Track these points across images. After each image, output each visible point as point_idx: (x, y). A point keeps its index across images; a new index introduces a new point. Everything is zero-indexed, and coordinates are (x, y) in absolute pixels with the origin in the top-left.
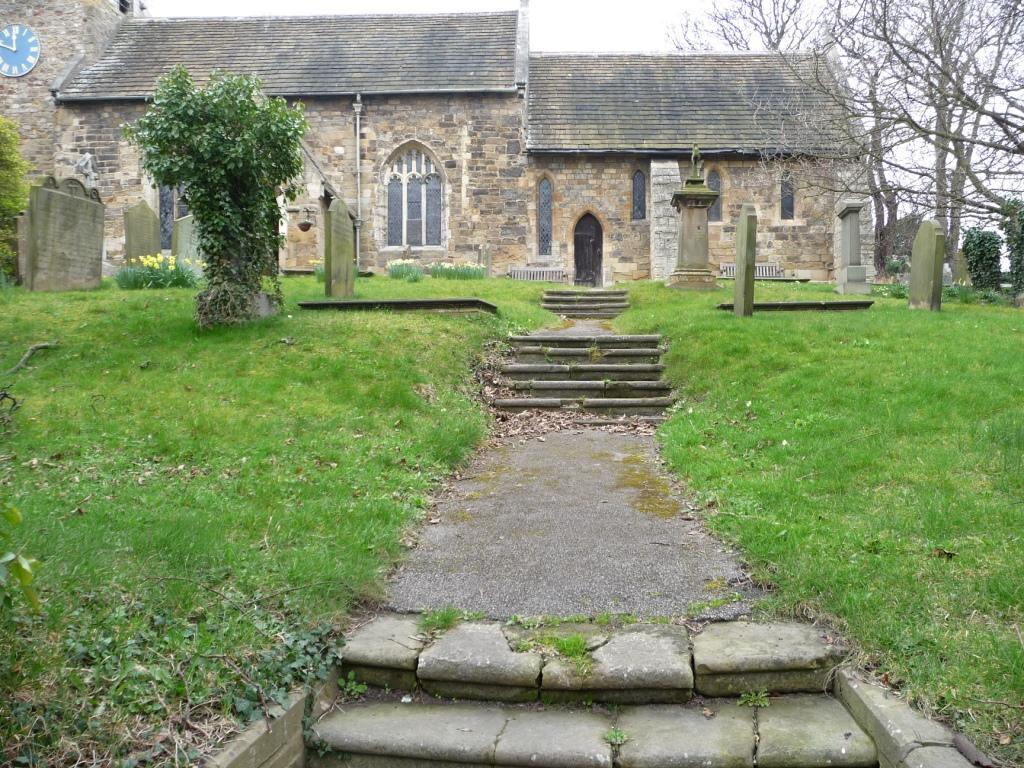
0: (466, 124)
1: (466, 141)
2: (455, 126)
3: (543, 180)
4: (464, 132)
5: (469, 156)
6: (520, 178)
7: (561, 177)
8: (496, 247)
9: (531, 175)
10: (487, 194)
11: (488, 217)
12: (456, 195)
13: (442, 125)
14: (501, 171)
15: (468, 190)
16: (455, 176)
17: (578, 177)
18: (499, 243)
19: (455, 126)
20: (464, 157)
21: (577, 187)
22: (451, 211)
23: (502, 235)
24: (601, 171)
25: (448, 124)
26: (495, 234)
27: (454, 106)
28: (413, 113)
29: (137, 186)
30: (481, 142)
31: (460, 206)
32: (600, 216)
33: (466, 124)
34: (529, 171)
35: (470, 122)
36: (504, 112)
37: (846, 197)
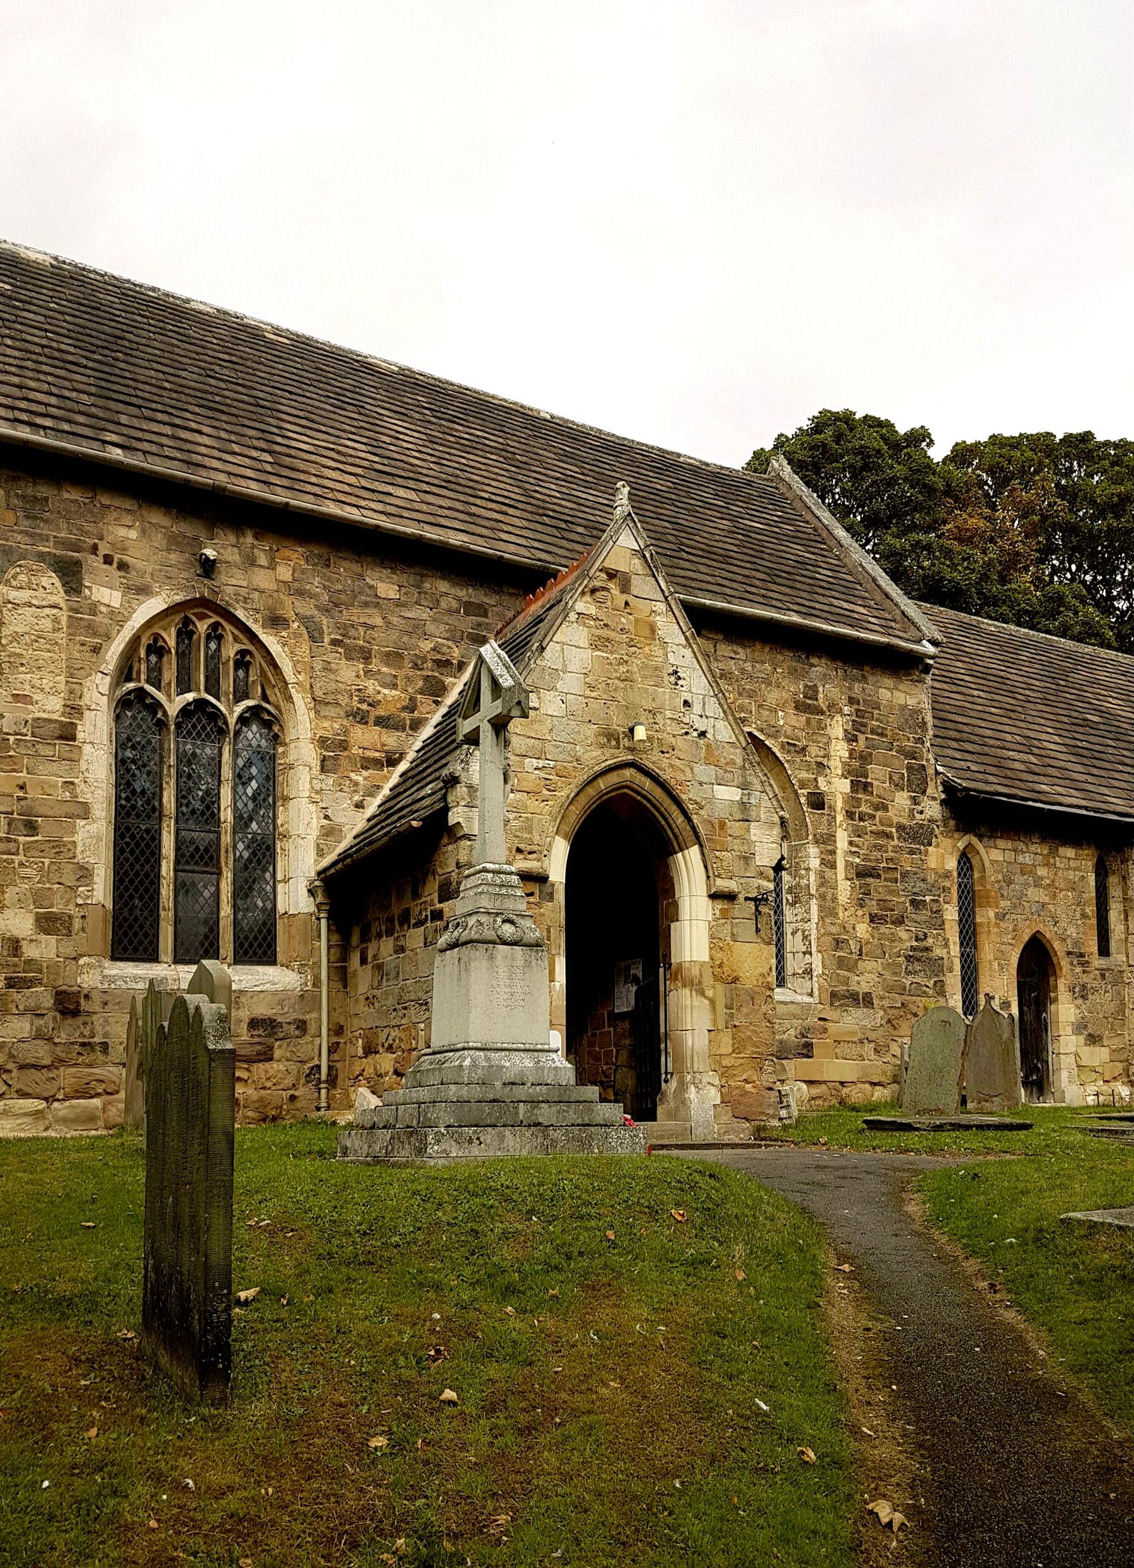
0: (840, 712)
1: (840, 750)
2: (822, 713)
3: (965, 860)
4: (837, 727)
5: (844, 786)
6: (930, 849)
7: (996, 855)
8: (898, 1000)
9: (946, 842)
10: (879, 876)
11: (883, 929)
12: (829, 873)
13: (799, 707)
14: (901, 828)
15: (848, 864)
16: (823, 829)
17: (1020, 859)
18: (902, 991)
19: (822, 713)
20: (838, 787)
21: (1019, 879)
22: (821, 908)
23: (908, 973)
24: (1053, 853)
25: (806, 706)
26: (892, 967)
27: (820, 668)
28: (748, 666)
29: (61, 747)
30: (865, 758)
31: (834, 899)
32: (1057, 945)
33: (840, 712)
34: (947, 834)
35: (846, 710)
36: (900, 698)
37: (281, 997)
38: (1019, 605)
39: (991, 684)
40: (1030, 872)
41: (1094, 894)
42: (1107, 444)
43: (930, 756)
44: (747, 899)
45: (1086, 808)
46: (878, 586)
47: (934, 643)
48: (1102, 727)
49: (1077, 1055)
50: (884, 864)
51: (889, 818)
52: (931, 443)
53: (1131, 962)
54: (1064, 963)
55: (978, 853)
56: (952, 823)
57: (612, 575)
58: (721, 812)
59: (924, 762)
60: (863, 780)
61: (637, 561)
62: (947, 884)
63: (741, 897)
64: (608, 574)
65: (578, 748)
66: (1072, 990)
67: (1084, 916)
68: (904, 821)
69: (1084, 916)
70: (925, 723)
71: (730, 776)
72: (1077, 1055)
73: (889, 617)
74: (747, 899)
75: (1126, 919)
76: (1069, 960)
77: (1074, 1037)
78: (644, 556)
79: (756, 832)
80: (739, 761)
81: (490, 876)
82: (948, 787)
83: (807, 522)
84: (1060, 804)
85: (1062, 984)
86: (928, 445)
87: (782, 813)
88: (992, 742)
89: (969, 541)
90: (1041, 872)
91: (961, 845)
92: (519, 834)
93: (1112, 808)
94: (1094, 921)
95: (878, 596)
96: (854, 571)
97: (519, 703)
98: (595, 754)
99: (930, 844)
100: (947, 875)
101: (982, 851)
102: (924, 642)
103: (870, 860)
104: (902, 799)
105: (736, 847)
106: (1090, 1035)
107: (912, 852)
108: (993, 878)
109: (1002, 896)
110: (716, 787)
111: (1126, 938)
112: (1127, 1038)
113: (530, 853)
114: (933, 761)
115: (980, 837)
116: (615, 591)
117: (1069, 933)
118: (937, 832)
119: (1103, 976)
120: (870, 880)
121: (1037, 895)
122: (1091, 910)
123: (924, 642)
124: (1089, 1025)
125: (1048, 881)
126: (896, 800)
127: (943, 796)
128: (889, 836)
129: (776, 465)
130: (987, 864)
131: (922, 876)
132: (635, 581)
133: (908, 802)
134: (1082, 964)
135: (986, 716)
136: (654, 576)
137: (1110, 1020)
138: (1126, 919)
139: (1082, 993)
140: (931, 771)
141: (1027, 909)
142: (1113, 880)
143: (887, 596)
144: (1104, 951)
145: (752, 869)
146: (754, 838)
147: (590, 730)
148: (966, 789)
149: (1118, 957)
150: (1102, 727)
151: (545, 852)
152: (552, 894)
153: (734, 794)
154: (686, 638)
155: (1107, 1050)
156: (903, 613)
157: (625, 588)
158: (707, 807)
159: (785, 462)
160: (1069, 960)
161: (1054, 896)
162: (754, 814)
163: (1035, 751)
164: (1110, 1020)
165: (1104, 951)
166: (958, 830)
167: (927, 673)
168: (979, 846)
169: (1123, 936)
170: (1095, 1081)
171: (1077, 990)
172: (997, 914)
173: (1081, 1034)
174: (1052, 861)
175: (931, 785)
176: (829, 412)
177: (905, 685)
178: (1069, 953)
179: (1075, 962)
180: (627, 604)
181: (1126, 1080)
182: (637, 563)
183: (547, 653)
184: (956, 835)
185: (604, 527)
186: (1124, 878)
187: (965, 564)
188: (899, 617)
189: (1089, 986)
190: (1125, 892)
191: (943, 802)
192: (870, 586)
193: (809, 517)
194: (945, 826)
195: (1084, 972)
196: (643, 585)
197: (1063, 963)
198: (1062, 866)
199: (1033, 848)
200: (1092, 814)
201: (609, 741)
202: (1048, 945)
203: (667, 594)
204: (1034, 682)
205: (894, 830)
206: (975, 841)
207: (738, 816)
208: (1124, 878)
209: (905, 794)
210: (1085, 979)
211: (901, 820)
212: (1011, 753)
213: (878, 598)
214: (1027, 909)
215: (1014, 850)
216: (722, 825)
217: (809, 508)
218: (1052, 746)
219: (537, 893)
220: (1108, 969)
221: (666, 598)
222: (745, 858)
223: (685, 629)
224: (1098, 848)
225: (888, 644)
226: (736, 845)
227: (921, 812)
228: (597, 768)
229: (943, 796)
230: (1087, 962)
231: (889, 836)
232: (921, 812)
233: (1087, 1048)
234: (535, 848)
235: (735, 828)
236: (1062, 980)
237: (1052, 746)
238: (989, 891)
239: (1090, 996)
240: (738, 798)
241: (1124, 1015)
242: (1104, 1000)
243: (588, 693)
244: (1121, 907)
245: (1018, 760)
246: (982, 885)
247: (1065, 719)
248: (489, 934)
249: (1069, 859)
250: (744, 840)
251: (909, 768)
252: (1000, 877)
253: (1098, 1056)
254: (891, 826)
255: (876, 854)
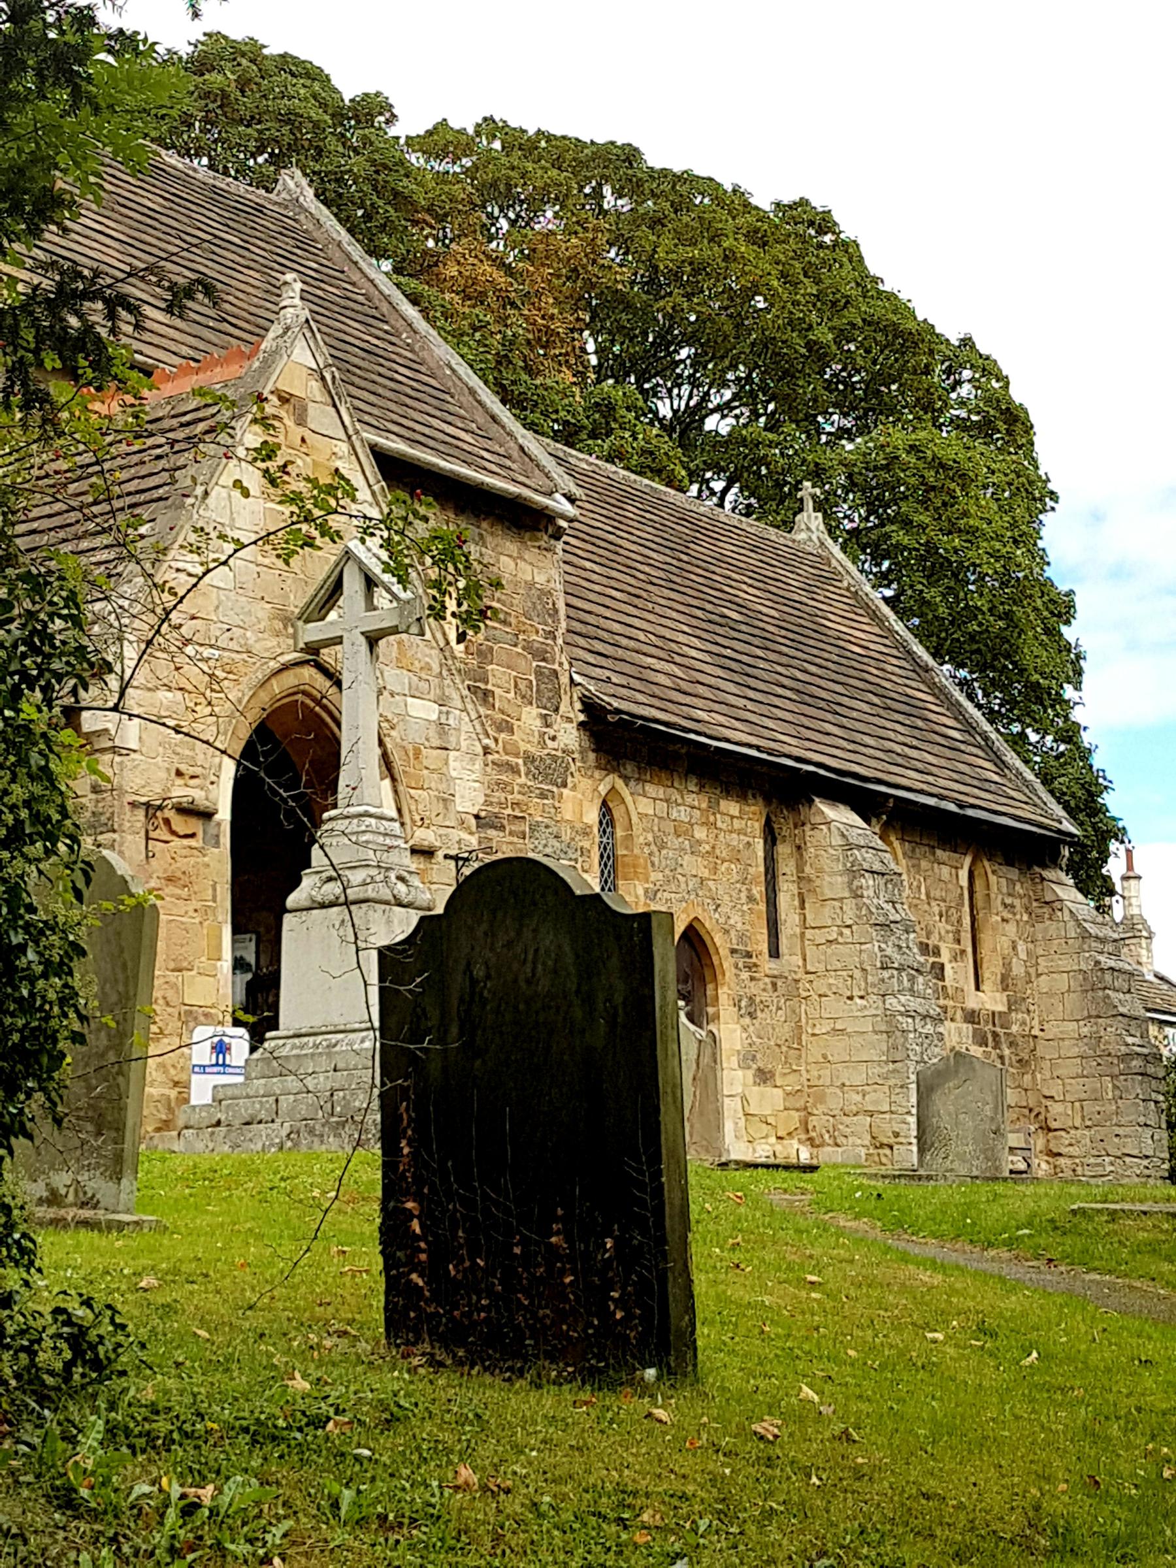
6: (565, 791)
7: (645, 806)
9: (585, 784)
10: (502, 828)
14: (529, 759)
21: (673, 841)
24: (713, 807)
32: (718, 939)
36: (526, 572)
38: (557, 412)
39: (601, 552)
40: (686, 833)
41: (762, 869)
42: (665, 173)
43: (564, 660)
44: (446, 857)
45: (758, 748)
46: (479, 402)
47: (571, 499)
48: (743, 628)
49: (744, 1098)
50: (509, 811)
51: (515, 744)
52: (392, 119)
53: (810, 968)
54: (727, 963)
55: (623, 801)
56: (592, 756)
57: (285, 399)
58: (415, 735)
59: (556, 667)
60: (482, 686)
61: (314, 383)
62: (586, 844)
63: (440, 854)
64: (280, 398)
65: (249, 634)
66: (737, 1004)
67: (751, 899)
68: (534, 750)
69: (751, 899)
70: (556, 611)
71: (425, 685)
72: (744, 1098)
73: (502, 451)
74: (446, 857)
75: (803, 907)
76: (732, 961)
77: (740, 1073)
78: (323, 378)
79: (456, 765)
80: (436, 668)
81: (373, 821)
82: (590, 707)
83: (353, 284)
84: (728, 740)
85: (723, 992)
86: (387, 122)
87: (486, 741)
88: (624, 642)
89: (481, 298)
90: (700, 833)
91: (603, 789)
92: (178, 749)
93: (787, 749)
94: (762, 907)
95: (481, 418)
96: (439, 373)
97: (419, 620)
98: (269, 644)
99: (565, 785)
100: (586, 831)
101: (629, 799)
102: (557, 496)
103: (491, 804)
104: (530, 717)
105: (433, 785)
106: (759, 1069)
107: (543, 796)
108: (641, 840)
109: (653, 864)
110: (410, 700)
111: (803, 934)
112: (805, 1075)
113: (192, 777)
114: (566, 666)
115: (626, 779)
116: (289, 422)
117: (732, 922)
118: (573, 768)
119: (774, 985)
120: (492, 833)
121: (693, 865)
122: (759, 890)
123: (557, 496)
124: (759, 1056)
125: (708, 848)
126: (523, 717)
127: (582, 717)
128: (515, 770)
129: (291, 184)
130: (635, 819)
131: (555, 830)
132: (313, 410)
133: (538, 722)
134: (749, 968)
135: (608, 602)
136: (335, 406)
137: (784, 1049)
138: (803, 907)
139: (750, 1009)
140: (564, 680)
141: (683, 886)
142: (783, 850)
143: (494, 418)
144: (775, 953)
145: (452, 815)
146: (454, 774)
147: (262, 611)
148: (618, 711)
149: (790, 959)
150: (743, 628)
151: (214, 778)
152: (218, 836)
153: (431, 711)
154: (373, 493)
155: (779, 1092)
156: (521, 448)
157: (301, 422)
158: (400, 727)
159: (304, 182)
160: (732, 961)
161: (715, 870)
162: (453, 739)
163: (678, 659)
164: (784, 1049)
165: (775, 953)
166: (598, 767)
167: (558, 539)
168: (625, 792)
169: (798, 930)
170: (766, 1137)
171: (743, 1004)
172: (646, 891)
173: (749, 1068)
174: (712, 819)
175: (565, 699)
176: (225, 38)
177: (531, 554)
178: (733, 951)
179: (741, 965)
180: (303, 440)
181: (804, 1137)
182: (315, 385)
183: (211, 501)
184: (597, 774)
185: (266, 324)
186: (799, 848)
187: (478, 336)
188: (515, 454)
189: (758, 1000)
190: (800, 868)
191: (581, 725)
192: (467, 399)
193: (356, 277)
194: (583, 760)
195: (752, 979)
196: (321, 417)
197: (726, 965)
198: (724, 826)
199: (690, 799)
200: (764, 756)
201: (285, 627)
202: (706, 938)
203: (351, 432)
204: (654, 555)
205: (520, 761)
206: (620, 784)
207: (436, 742)
208: (799, 848)
209: (535, 711)
210: (754, 989)
211: (529, 747)
212: (650, 660)
213: (481, 420)
214: (683, 886)
215: (667, 801)
216: (417, 754)
217: (356, 263)
218: (694, 653)
219: (200, 835)
220: (781, 976)
221: (349, 437)
222: (444, 800)
223: (372, 481)
224: (768, 801)
225: (519, 496)
226: (432, 780)
227: (554, 738)
228: (272, 664)
229: (582, 717)
230: (756, 965)
231: (515, 770)
232: (554, 738)
233: (756, 1088)
234: (197, 771)
235: (431, 757)
236: (725, 989)
237: (694, 653)
238: (637, 857)
239: (759, 1013)
240: (434, 717)
241: (800, 1043)
242: (775, 1020)
243: (260, 558)
244: (794, 888)
245: (664, 673)
246: (627, 848)
247: (699, 613)
248: (386, 894)
249: (732, 817)
250: (443, 775)
251: (539, 672)
252: (650, 838)
253: (770, 1100)
254: (517, 755)
255: (499, 795)
